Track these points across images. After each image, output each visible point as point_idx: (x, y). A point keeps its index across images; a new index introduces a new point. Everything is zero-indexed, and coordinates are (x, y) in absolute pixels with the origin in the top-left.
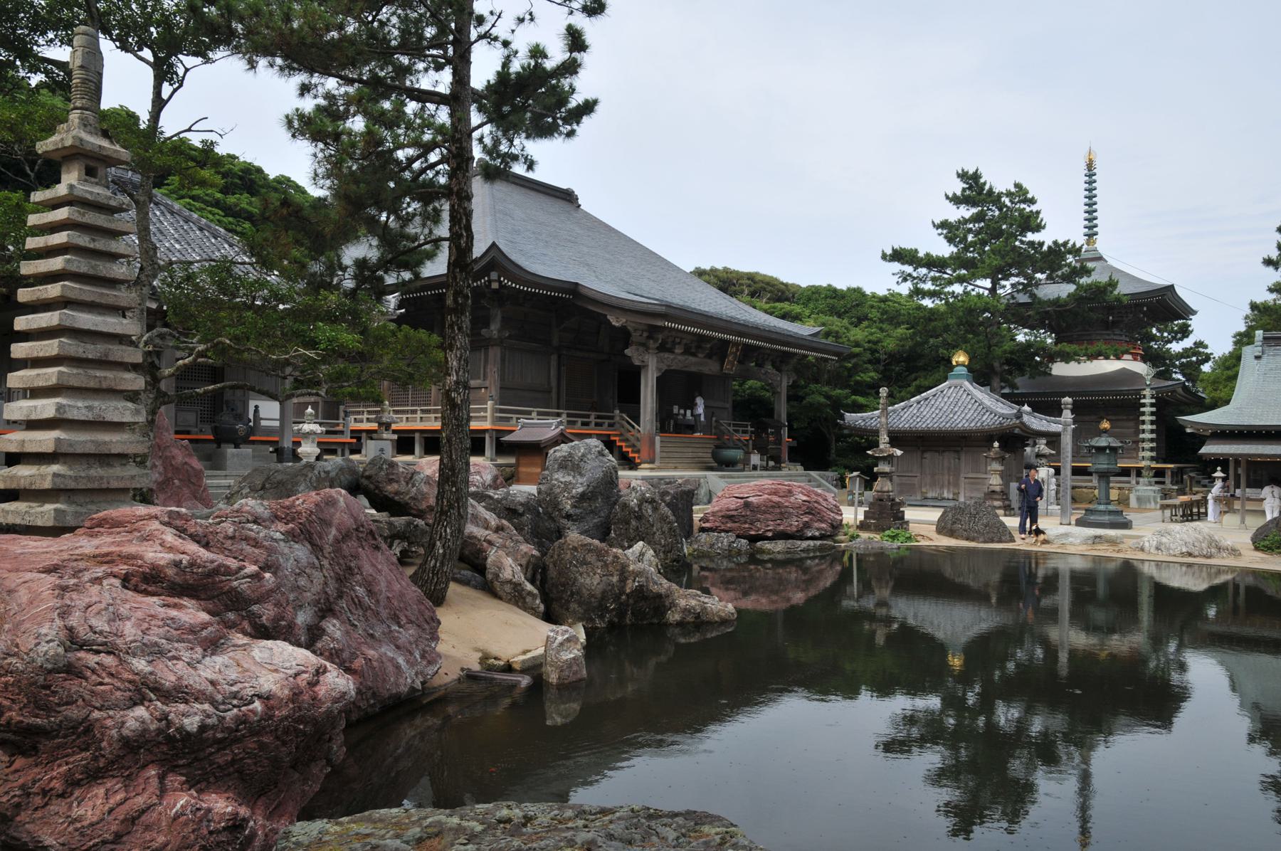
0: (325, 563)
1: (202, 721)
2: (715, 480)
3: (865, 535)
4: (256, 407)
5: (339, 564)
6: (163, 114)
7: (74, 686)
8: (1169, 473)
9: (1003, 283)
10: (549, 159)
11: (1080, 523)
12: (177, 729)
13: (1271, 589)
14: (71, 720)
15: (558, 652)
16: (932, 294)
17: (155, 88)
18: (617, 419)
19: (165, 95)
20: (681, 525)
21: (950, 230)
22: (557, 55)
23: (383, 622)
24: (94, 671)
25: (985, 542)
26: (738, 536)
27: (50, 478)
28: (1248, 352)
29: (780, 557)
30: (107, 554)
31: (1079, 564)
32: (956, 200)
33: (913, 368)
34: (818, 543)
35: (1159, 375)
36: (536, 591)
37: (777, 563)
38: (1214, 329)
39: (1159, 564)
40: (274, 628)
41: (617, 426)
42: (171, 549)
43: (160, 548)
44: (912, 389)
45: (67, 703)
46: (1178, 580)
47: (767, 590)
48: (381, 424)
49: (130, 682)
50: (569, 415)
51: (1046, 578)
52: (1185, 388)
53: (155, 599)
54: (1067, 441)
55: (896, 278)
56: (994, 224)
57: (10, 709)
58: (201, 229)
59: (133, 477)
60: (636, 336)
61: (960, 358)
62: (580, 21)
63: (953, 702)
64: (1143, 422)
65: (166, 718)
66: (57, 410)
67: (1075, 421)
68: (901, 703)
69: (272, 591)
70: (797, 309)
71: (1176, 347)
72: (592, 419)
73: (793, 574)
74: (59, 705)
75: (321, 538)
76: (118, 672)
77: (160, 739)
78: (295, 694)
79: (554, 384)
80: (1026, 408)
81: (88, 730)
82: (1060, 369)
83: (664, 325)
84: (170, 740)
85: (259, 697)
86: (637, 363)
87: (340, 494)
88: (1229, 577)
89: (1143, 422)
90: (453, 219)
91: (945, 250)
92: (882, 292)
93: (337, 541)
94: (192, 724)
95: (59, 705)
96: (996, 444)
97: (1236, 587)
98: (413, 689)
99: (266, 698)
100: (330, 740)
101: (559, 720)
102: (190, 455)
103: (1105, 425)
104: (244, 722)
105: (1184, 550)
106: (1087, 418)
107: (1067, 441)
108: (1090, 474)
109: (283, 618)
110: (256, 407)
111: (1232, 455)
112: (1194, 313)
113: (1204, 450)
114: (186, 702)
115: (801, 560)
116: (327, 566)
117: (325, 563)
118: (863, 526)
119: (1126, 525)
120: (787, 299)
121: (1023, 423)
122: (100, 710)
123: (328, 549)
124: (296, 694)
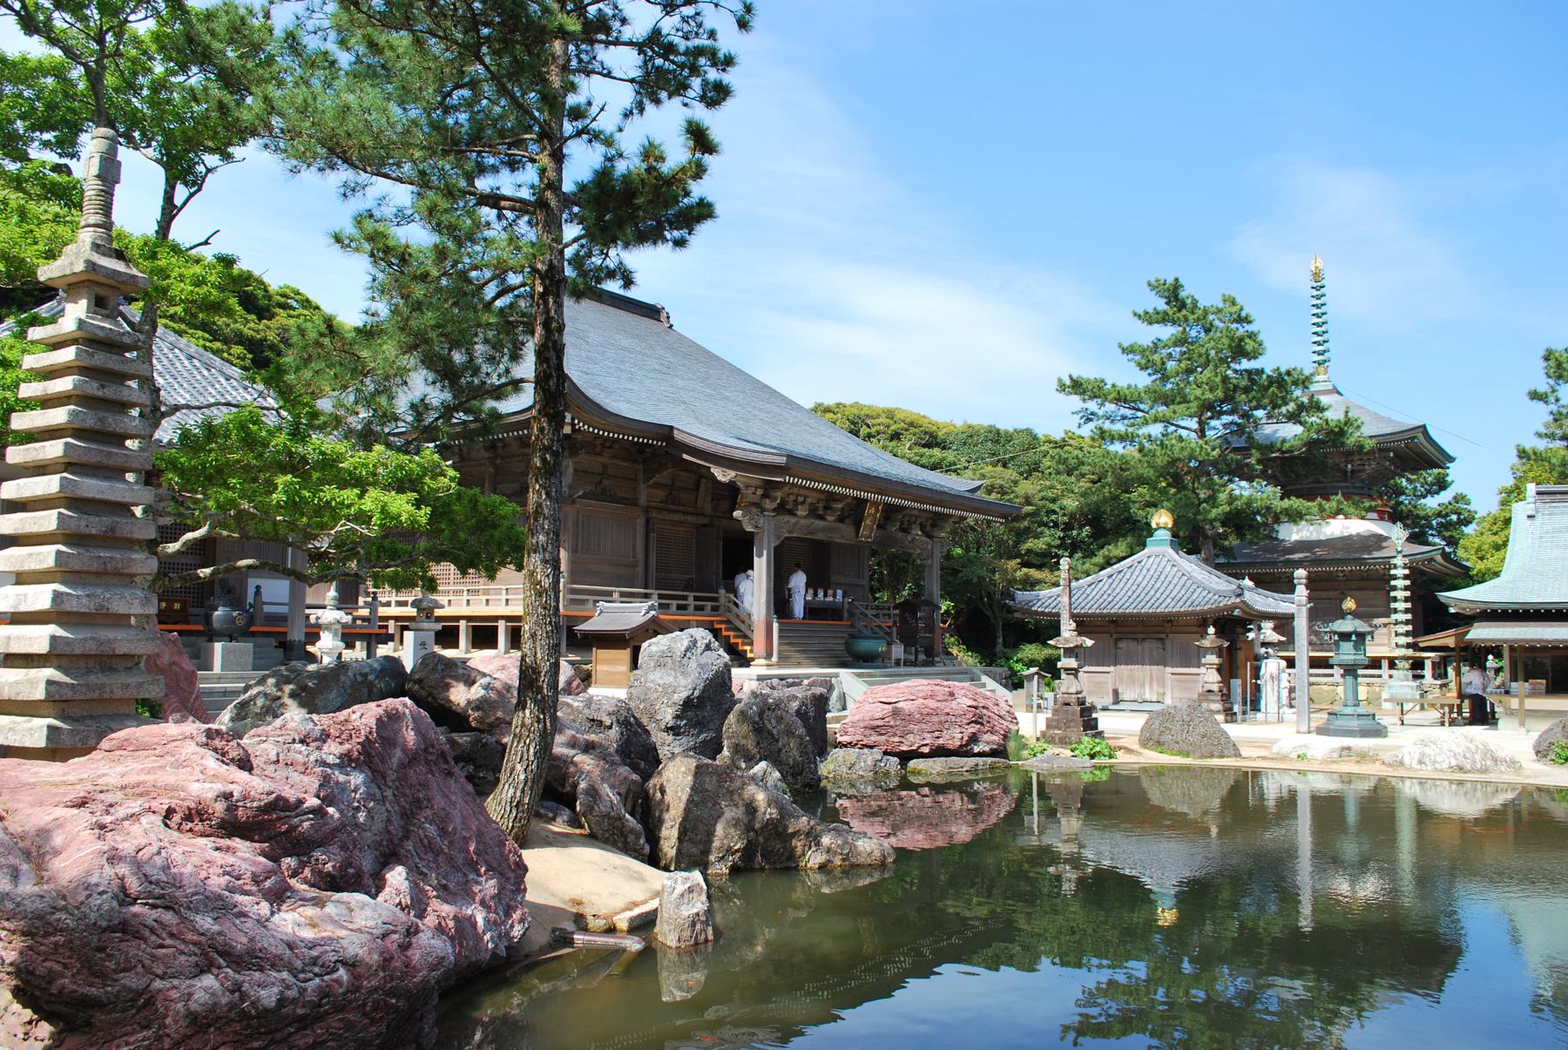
0: (389, 793)
1: (281, 993)
2: (848, 681)
3: (1052, 750)
4: (258, 587)
5: (404, 795)
6: (174, 224)
7: (133, 949)
8: (1428, 664)
9: (1213, 423)
10: (651, 268)
11: (1322, 731)
12: (253, 1003)
13: (1559, 810)
14: (130, 990)
15: (678, 906)
16: (1123, 438)
17: (166, 192)
19: (178, 201)
20: (814, 741)
21: (1147, 358)
22: (677, 154)
23: (458, 869)
24: (152, 931)
25: (1202, 757)
26: (886, 753)
27: (43, 685)
28: (1519, 510)
29: (939, 780)
30: (138, 785)
31: (1324, 785)
32: (1150, 318)
33: (1107, 527)
34: (989, 760)
35: (1413, 539)
36: (639, 827)
38: (1476, 478)
39: (1422, 782)
40: (342, 877)
41: (722, 609)
42: (215, 777)
43: (201, 777)
44: (1099, 559)
45: (125, 970)
46: (1448, 802)
47: (921, 821)
48: (420, 610)
49: (195, 944)
50: (696, 599)
51: (1280, 802)
52: (1445, 556)
53: (204, 841)
54: (1301, 625)
55: (1077, 419)
57: (63, 976)
58: (190, 358)
59: (141, 685)
60: (749, 495)
61: (1162, 519)
62: (700, 113)
63: (1165, 970)
64: (1395, 599)
65: (239, 990)
66: (54, 600)
67: (1310, 599)
68: (1095, 975)
69: (336, 830)
70: (950, 456)
71: (1432, 503)
72: (691, 602)
73: (956, 802)
74: (115, 971)
75: (383, 762)
76: (181, 933)
77: (232, 1015)
78: (385, 960)
79: (640, 555)
80: (1247, 582)
81: (150, 1002)
82: (1292, 533)
83: (783, 479)
84: (244, 1015)
85: (344, 963)
86: (749, 529)
87: (405, 705)
88: (1510, 796)
89: (1395, 599)
90: (541, 355)
91: (1143, 380)
92: (1058, 435)
93: (402, 766)
94: (268, 996)
95: (115, 971)
97: (1518, 813)
98: (495, 955)
99: (351, 964)
100: (422, 1017)
101: (679, 995)
102: (180, 653)
103: (1349, 604)
104: (327, 995)
105: (1454, 763)
106: (1324, 594)
107: (1301, 625)
108: (1331, 667)
109: (350, 865)
110: (258, 587)
111: (1506, 641)
112: (1452, 459)
114: (261, 969)
115: (969, 783)
116: (390, 797)
117: (389, 793)
118: (1044, 737)
119: (1379, 732)
120: (937, 445)
121: (1244, 602)
122: (162, 978)
123: (392, 776)
124: (387, 960)
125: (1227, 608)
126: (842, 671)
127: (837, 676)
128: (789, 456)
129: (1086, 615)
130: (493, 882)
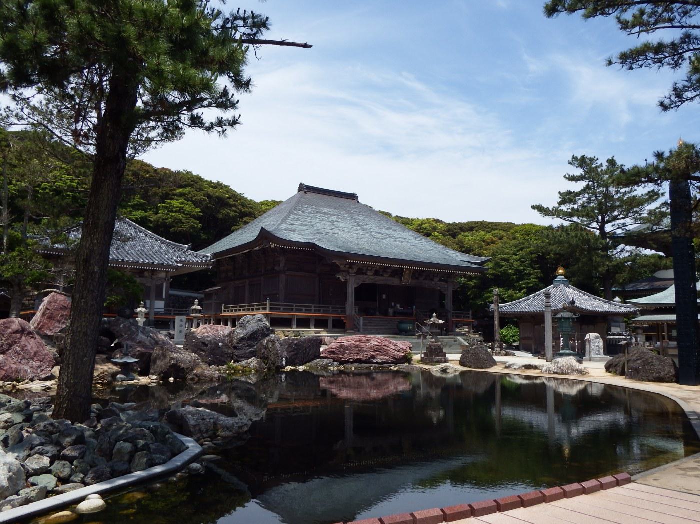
26: (334, 361)
37: (355, 374)
50: (333, 308)
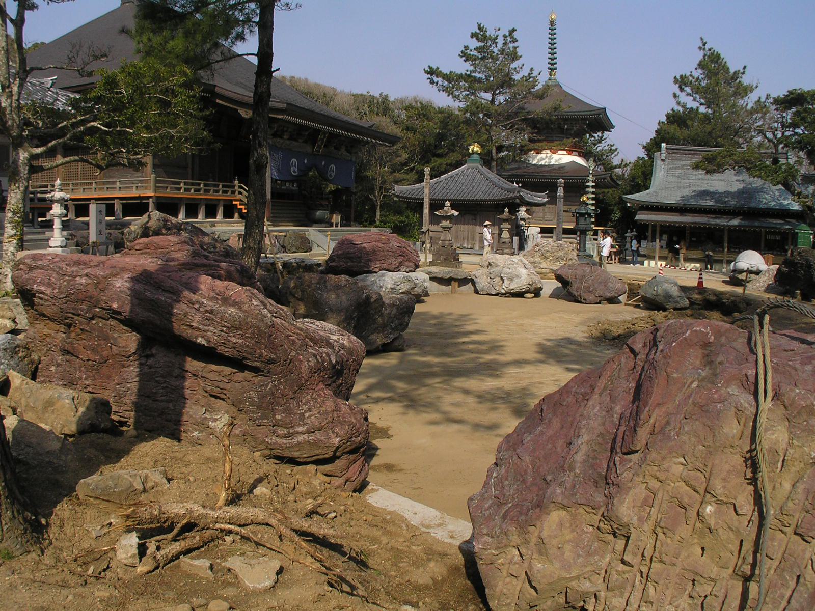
18: (236, 188)
50: (185, 184)
56: (491, 55)
91: (463, 67)
96: (506, 210)
113: (637, 218)
125: (512, 198)
126: (311, 229)
127: (308, 231)
128: (288, 104)
129: (455, 200)
130: (608, 241)
